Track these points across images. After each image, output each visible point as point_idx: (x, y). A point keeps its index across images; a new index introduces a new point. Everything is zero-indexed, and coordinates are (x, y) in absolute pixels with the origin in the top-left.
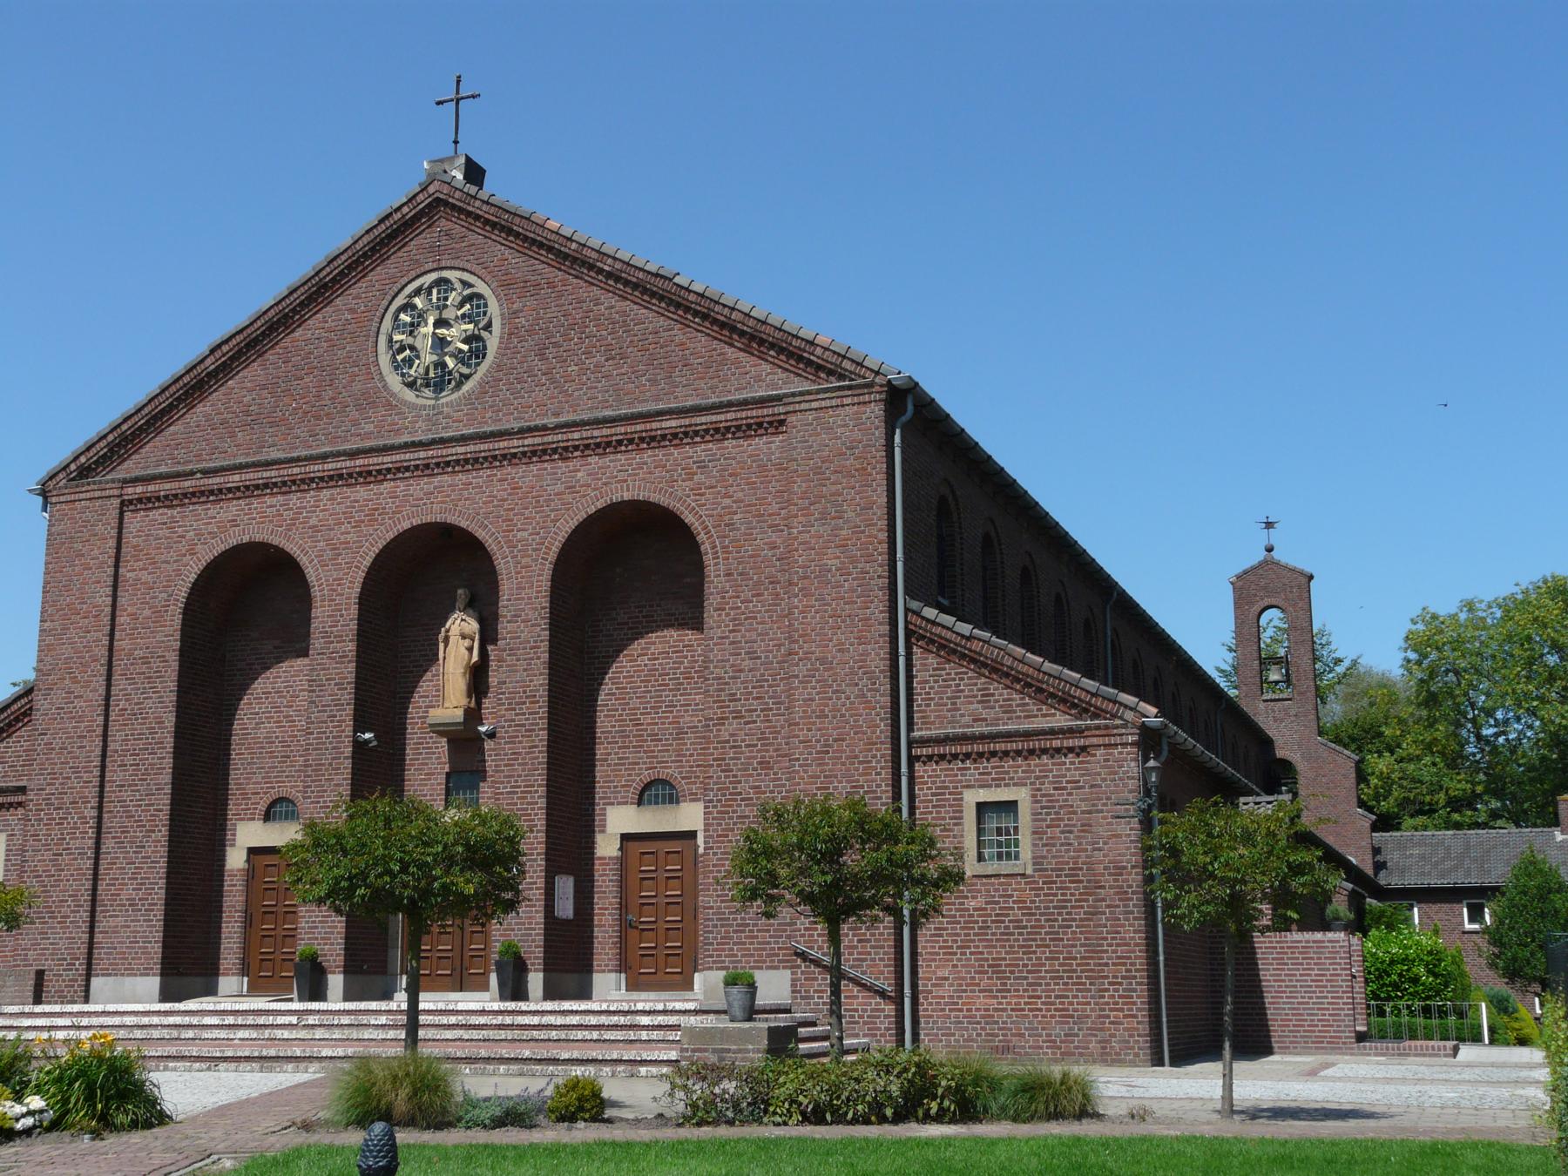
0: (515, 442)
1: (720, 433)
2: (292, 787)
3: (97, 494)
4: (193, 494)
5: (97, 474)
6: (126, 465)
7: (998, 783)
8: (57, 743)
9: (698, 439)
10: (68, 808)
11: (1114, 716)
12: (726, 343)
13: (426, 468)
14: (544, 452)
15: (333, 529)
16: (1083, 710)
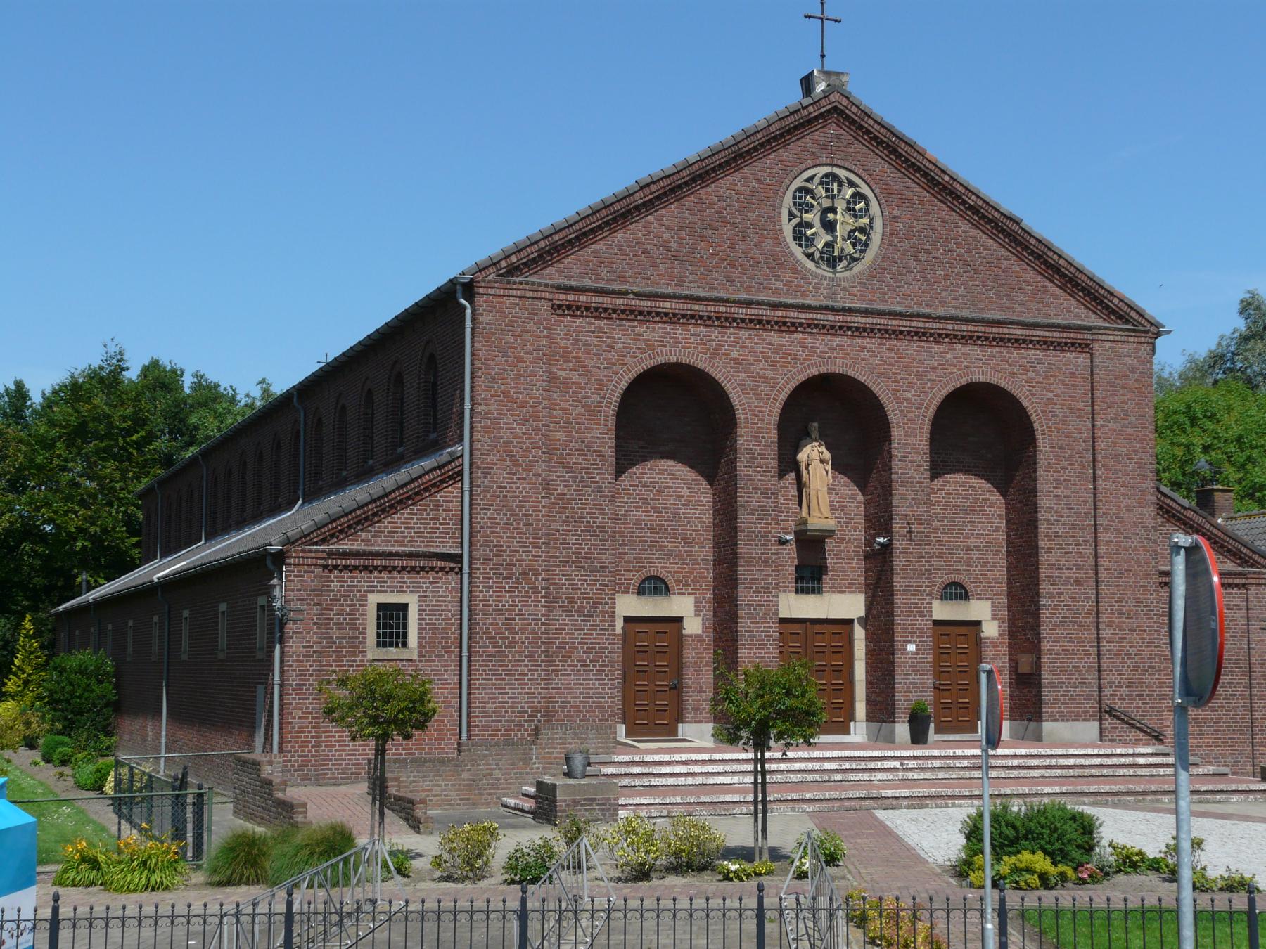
0: (905, 323)
1: (1045, 344)
2: (662, 568)
3: (528, 294)
4: (623, 311)
5: (522, 274)
6: (547, 271)
8: (502, 519)
9: (1031, 346)
10: (517, 579)
13: (832, 329)
14: (924, 334)
15: (753, 364)
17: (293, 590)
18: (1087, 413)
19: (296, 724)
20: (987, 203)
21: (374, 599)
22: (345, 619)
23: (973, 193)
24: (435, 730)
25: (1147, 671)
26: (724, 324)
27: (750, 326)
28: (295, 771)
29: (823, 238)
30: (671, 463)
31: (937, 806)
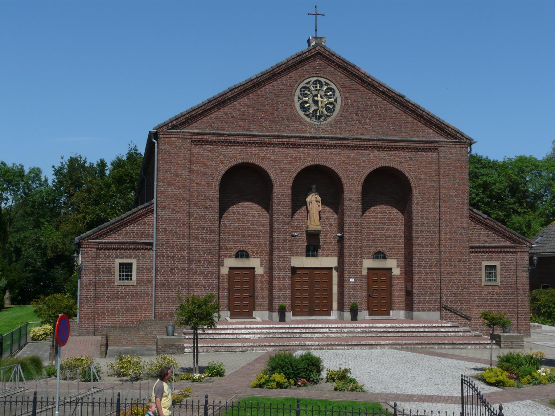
0: (350, 142)
1: (417, 149)
2: (246, 247)
3: (181, 136)
4: (223, 142)
5: (179, 128)
6: (190, 126)
7: (491, 260)
8: (169, 228)
9: (410, 150)
10: (176, 253)
11: (524, 244)
12: (418, 121)
13: (316, 146)
14: (359, 147)
16: (515, 241)
17: (84, 258)
18: (437, 179)
19: (85, 311)
20: (389, 90)
21: (118, 261)
22: (106, 269)
23: (382, 86)
24: (143, 314)
25: (463, 290)
26: (268, 146)
27: (279, 146)
28: (84, 329)
29: (314, 107)
30: (251, 203)
31: (328, 349)
